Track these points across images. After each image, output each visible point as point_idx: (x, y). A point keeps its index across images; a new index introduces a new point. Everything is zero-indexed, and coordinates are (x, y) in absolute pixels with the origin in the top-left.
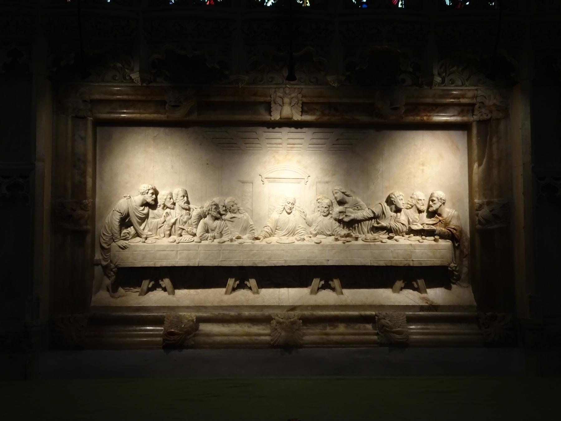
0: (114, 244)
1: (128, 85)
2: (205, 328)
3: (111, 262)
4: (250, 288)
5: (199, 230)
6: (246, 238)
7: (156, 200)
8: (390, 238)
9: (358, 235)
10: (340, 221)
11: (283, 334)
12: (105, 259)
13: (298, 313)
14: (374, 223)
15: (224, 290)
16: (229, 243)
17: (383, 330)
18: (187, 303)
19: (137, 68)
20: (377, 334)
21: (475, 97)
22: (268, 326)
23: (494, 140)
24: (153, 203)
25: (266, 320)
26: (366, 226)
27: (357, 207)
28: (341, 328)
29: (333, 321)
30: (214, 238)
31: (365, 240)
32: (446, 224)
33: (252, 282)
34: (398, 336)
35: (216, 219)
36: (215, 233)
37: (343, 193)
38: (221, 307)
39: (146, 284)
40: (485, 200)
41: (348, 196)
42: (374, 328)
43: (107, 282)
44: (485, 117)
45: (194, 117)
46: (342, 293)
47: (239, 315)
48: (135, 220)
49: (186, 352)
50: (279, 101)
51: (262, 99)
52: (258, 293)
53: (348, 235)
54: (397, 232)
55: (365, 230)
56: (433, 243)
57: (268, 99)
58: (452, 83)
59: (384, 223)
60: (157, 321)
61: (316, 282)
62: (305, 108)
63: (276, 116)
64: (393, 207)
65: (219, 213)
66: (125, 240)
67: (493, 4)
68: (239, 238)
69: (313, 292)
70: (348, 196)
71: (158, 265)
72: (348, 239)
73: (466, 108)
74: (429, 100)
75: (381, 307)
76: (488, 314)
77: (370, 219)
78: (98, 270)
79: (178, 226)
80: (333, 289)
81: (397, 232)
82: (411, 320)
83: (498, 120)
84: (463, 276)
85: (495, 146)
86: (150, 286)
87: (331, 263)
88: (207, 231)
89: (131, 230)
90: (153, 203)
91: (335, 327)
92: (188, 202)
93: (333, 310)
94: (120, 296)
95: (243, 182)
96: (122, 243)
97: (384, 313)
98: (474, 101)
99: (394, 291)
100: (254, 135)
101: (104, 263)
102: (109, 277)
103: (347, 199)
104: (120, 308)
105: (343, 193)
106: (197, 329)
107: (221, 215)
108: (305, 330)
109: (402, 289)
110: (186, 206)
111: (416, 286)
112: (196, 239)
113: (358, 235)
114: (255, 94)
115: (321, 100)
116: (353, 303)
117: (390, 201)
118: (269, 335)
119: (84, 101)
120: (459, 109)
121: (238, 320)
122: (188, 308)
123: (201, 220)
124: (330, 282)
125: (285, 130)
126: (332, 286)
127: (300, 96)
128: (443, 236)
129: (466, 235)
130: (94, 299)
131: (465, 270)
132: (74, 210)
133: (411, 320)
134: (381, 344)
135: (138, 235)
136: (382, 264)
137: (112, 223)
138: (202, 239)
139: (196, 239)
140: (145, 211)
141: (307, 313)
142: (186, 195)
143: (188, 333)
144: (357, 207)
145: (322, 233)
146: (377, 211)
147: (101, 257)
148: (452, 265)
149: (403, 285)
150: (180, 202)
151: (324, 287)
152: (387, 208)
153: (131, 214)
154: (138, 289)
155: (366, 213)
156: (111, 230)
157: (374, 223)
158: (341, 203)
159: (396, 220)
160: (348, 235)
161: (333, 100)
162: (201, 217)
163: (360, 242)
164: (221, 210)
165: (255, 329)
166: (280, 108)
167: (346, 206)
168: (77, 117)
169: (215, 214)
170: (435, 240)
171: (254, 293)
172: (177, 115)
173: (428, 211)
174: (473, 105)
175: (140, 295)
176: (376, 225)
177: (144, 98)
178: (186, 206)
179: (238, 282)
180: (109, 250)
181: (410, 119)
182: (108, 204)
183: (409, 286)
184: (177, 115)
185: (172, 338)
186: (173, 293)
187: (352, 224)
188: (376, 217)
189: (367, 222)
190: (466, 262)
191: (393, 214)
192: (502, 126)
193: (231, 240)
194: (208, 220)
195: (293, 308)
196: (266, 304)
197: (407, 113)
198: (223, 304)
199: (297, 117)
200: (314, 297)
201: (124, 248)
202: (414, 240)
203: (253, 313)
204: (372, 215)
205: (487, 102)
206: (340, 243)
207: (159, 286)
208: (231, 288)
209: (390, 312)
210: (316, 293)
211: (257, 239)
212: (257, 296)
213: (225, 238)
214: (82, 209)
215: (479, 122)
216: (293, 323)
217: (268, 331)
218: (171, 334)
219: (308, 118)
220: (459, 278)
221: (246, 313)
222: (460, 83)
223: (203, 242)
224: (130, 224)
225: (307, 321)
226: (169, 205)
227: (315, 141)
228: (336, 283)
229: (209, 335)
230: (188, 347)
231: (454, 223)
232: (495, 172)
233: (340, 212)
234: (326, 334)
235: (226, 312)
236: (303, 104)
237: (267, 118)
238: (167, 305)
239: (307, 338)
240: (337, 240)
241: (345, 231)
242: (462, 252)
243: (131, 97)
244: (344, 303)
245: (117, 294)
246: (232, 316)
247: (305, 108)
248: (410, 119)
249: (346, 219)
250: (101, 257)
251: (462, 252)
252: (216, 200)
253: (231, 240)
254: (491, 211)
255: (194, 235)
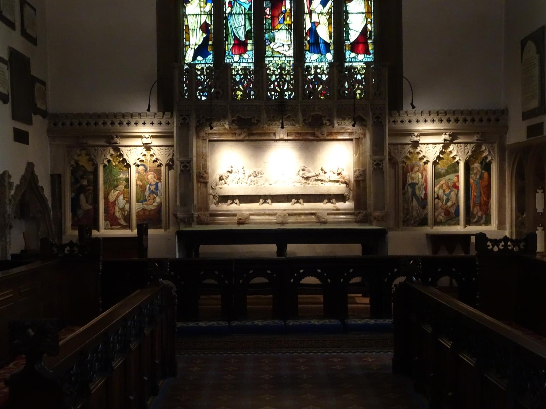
0: (217, 187)
1: (360, 305)
2: (251, 217)
3: (216, 193)
4: (268, 203)
5: (249, 181)
6: (267, 184)
7: (232, 170)
8: (322, 183)
9: (310, 182)
10: (303, 177)
11: (281, 219)
12: (214, 193)
13: (286, 212)
14: (316, 178)
15: (258, 204)
16: (260, 186)
17: (318, 217)
18: (245, 209)
19: (227, 123)
20: (316, 219)
21: (353, 129)
22: (275, 216)
23: (361, 146)
24: (231, 171)
25: (275, 214)
26: (313, 179)
27: (309, 171)
28: (303, 217)
29: (300, 214)
30: (254, 184)
31: (313, 184)
32: (344, 178)
33: (269, 201)
34: (323, 220)
35: (255, 177)
36: (255, 182)
37: (304, 166)
38: (258, 210)
39: (229, 202)
40: (358, 169)
41: (306, 167)
42: (315, 217)
43: (215, 201)
44: (357, 137)
45: (247, 138)
46: (303, 205)
47: (264, 213)
48: (224, 178)
49: (245, 225)
50: (279, 132)
51: (272, 132)
52: (271, 205)
53: (306, 183)
54: (325, 181)
55: (313, 180)
56: (339, 185)
57: (274, 132)
58: (345, 124)
59: (319, 178)
60: (235, 215)
61: (294, 201)
62: (289, 134)
63: (277, 138)
64: (323, 172)
65: (256, 175)
66: (221, 185)
67: (100, 302)
68: (264, 184)
69: (293, 204)
70: (306, 167)
71: (234, 194)
72: (306, 184)
73: (351, 133)
74: (336, 131)
75: (318, 209)
76: (358, 211)
77: (315, 176)
78: (211, 197)
79: (240, 180)
80: (300, 203)
81: (325, 181)
82: (328, 214)
83: (362, 138)
84: (350, 198)
85: (361, 149)
86: (231, 202)
87: (299, 193)
88: (252, 182)
89: (223, 181)
90: (231, 171)
91: (300, 217)
92: (244, 171)
93: (468, 360)
94: (220, 206)
95: (265, 163)
96: (220, 186)
97: (319, 212)
98: (353, 131)
99: (324, 204)
100: (269, 144)
101: (213, 194)
102: (215, 199)
103: (305, 168)
104: (220, 211)
105: (304, 166)
106: (249, 218)
107: (257, 175)
108: (289, 217)
109: (326, 203)
110: (244, 172)
111: (332, 202)
112: (248, 184)
113: (310, 182)
114: (270, 130)
115: (295, 132)
116: (308, 208)
117: (322, 169)
118: (276, 219)
119: (206, 134)
120: (348, 133)
121: (264, 214)
122: (245, 210)
123: (26, 245)
124: (299, 201)
125: (281, 142)
126: (300, 202)
127: (286, 130)
128: (342, 183)
129: (352, 182)
130: (210, 207)
131: (351, 195)
132: (204, 174)
133: (328, 214)
134: (317, 223)
135: (225, 183)
136: (319, 193)
137: (216, 178)
138: (250, 184)
139: (248, 184)
140: (228, 174)
141: (290, 212)
142: (243, 168)
143: (246, 219)
144: (309, 171)
145: (296, 182)
146: (317, 174)
147: (212, 192)
148: (346, 194)
149: (327, 201)
150: (241, 171)
151: (296, 203)
152: (321, 172)
153: (223, 176)
154: (226, 204)
155: (313, 174)
156: (216, 182)
157: (316, 178)
158: (303, 170)
159: (324, 177)
160: (306, 183)
161: (299, 132)
162: (250, 176)
163: (310, 185)
164: (257, 174)
165: (271, 218)
166: (279, 135)
167: (305, 171)
168: (203, 139)
169: (255, 175)
170: (340, 184)
171: (270, 205)
172: (240, 138)
173: (337, 174)
174: (353, 132)
175: (227, 206)
176: (317, 179)
177: (228, 132)
178: (244, 172)
179: (264, 201)
180: (215, 189)
181: (329, 138)
182: (214, 172)
183: (329, 201)
184: (240, 138)
185: (241, 220)
186: (240, 205)
187: (307, 178)
188: (317, 176)
189: (313, 177)
190: (351, 192)
191: (324, 174)
192: (363, 141)
193: (261, 185)
194: (252, 177)
195: (285, 210)
196: (275, 208)
197: (328, 135)
198: (259, 209)
199: (286, 138)
200: (292, 206)
201: (221, 188)
202: (332, 184)
203: (270, 212)
204: (315, 175)
205: (358, 132)
206: (302, 185)
207: (234, 202)
208: (261, 203)
209: (321, 211)
210: (293, 205)
211: (271, 184)
212: (271, 206)
213: (258, 184)
214: (206, 174)
215: (356, 139)
216: (285, 215)
217: (275, 218)
218: (240, 219)
219: (289, 138)
220: (349, 199)
221: (267, 212)
222: (348, 124)
223: (251, 186)
224: (223, 179)
225: (290, 215)
226: (237, 171)
227: (293, 146)
228: (301, 201)
229: (253, 220)
230: (246, 224)
231: (347, 178)
232: (361, 158)
233: (303, 174)
234: (297, 219)
235: (260, 212)
236: (288, 133)
237: (274, 138)
238: (237, 209)
239: (290, 221)
240: (301, 184)
241: (305, 181)
242: (350, 189)
243: (223, 132)
244: (304, 208)
245: (219, 205)
246: (262, 213)
247: (289, 134)
248: (329, 138)
249: (305, 177)
250: (212, 192)
251: (350, 189)
252: (255, 169)
253: (261, 185)
254: (359, 173)
255: (247, 183)
